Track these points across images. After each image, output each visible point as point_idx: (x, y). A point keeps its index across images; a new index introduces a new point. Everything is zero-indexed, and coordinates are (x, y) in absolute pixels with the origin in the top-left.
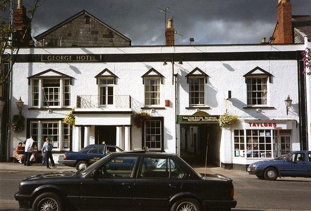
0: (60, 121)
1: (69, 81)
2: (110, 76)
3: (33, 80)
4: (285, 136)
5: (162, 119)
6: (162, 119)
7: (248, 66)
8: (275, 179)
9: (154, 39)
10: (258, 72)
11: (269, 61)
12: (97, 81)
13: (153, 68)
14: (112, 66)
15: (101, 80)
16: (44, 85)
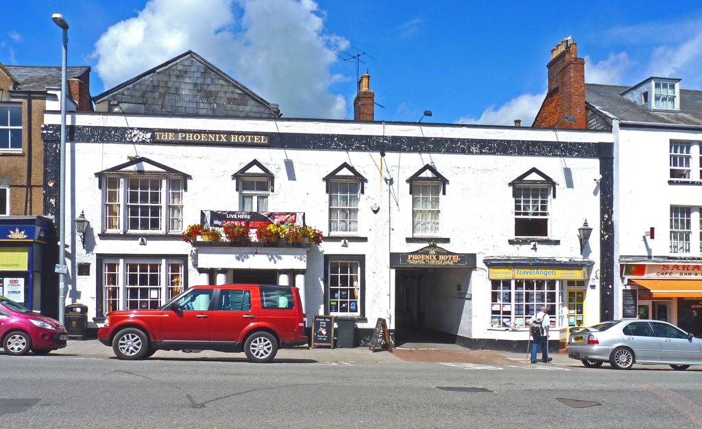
0: (164, 261)
1: (179, 180)
2: (542, 182)
3: (108, 179)
4: (575, 289)
5: (361, 259)
6: (361, 259)
7: (518, 165)
8: (271, 360)
9: (508, 114)
10: (534, 177)
11: (101, 144)
12: (237, 184)
13: (345, 163)
14: (444, 163)
15: (244, 182)
16: (168, 188)
